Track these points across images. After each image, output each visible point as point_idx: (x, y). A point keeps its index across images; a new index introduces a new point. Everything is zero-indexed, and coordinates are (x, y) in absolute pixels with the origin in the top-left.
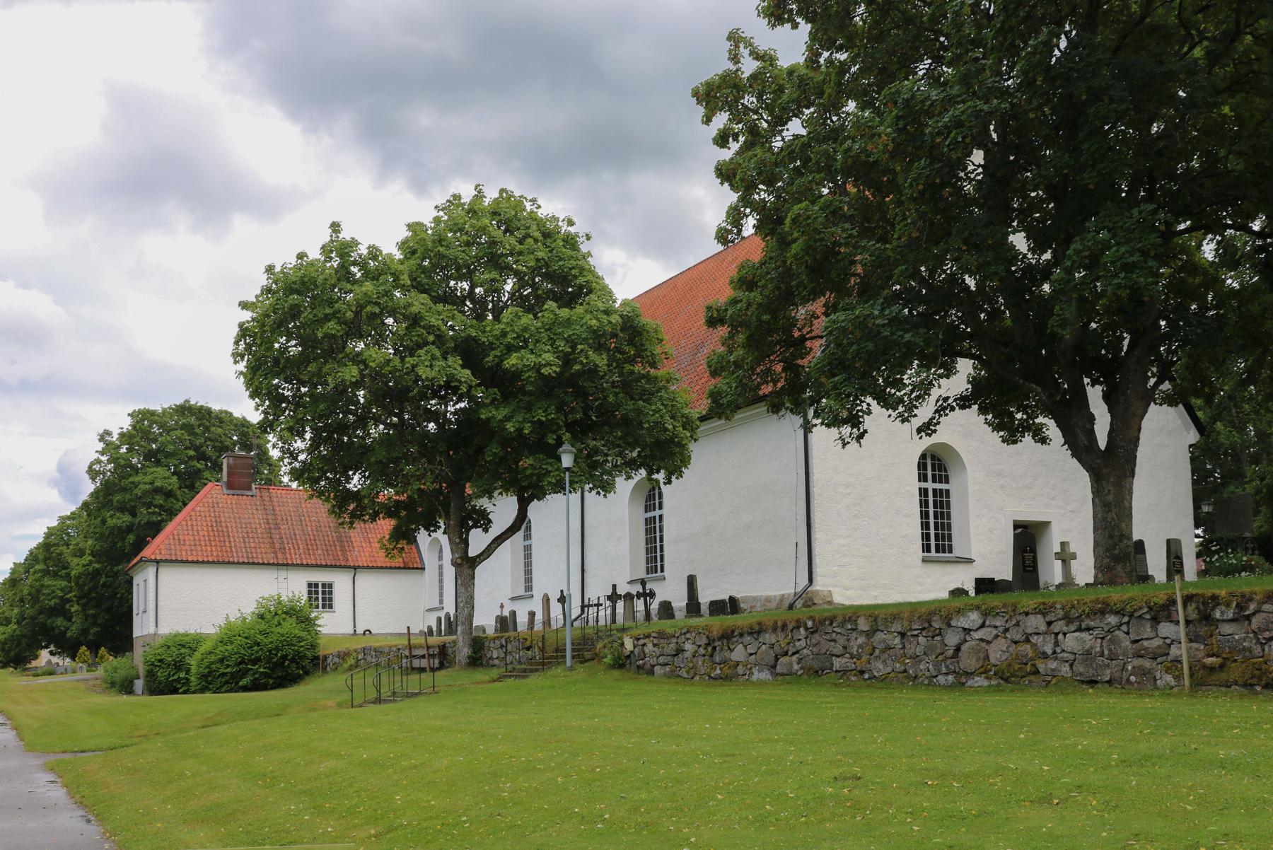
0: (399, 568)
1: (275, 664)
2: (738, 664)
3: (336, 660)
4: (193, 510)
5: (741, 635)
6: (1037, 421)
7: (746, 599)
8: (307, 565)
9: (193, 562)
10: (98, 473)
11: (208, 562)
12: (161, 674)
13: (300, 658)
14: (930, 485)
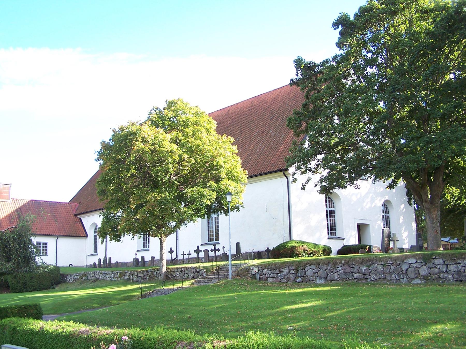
14: (329, 209)
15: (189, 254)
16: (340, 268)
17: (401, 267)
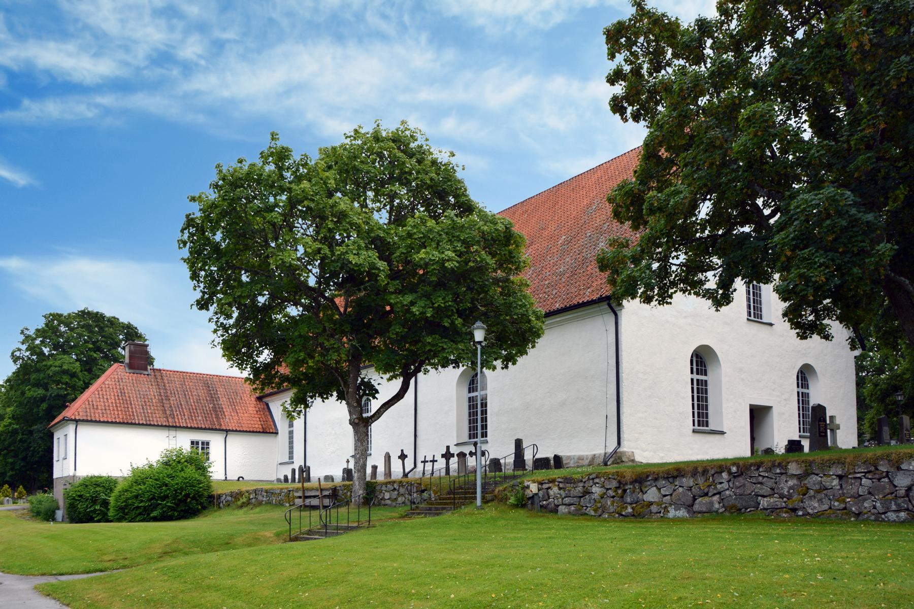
0: (259, 432)
1: (180, 500)
2: (651, 503)
3: (229, 498)
4: (103, 383)
5: (656, 479)
6: (824, 322)
7: (569, 457)
8: (191, 428)
9: (104, 422)
10: (19, 358)
11: (116, 423)
12: (81, 506)
13: (199, 496)
14: (696, 377)
15: (433, 461)
16: (725, 486)
17: (891, 482)
